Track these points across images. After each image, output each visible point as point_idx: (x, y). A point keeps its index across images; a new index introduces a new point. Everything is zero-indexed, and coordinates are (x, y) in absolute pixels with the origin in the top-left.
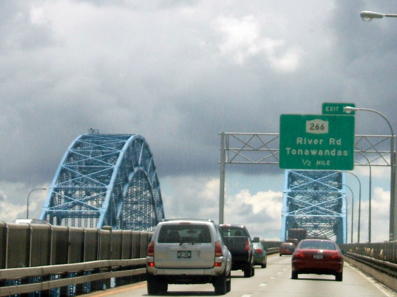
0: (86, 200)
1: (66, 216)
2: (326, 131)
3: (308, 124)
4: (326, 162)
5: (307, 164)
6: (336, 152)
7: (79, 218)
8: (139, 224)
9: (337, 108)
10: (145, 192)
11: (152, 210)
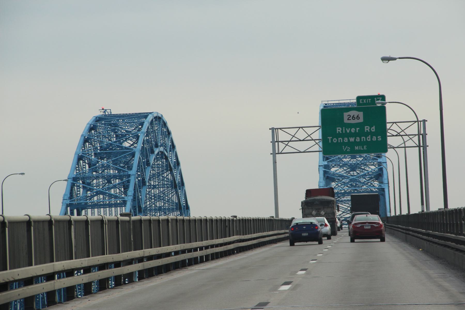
0: (109, 189)
1: (85, 207)
2: (361, 120)
3: (346, 115)
4: (363, 148)
5: (347, 149)
6: (372, 138)
7: (98, 209)
8: (160, 209)
9: (370, 100)
10: (108, 159)
11: (174, 193)
